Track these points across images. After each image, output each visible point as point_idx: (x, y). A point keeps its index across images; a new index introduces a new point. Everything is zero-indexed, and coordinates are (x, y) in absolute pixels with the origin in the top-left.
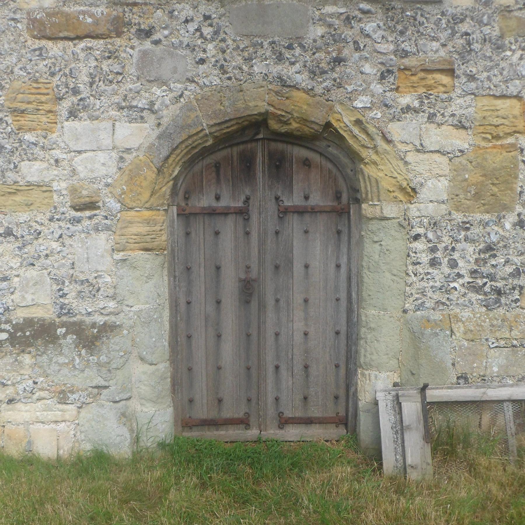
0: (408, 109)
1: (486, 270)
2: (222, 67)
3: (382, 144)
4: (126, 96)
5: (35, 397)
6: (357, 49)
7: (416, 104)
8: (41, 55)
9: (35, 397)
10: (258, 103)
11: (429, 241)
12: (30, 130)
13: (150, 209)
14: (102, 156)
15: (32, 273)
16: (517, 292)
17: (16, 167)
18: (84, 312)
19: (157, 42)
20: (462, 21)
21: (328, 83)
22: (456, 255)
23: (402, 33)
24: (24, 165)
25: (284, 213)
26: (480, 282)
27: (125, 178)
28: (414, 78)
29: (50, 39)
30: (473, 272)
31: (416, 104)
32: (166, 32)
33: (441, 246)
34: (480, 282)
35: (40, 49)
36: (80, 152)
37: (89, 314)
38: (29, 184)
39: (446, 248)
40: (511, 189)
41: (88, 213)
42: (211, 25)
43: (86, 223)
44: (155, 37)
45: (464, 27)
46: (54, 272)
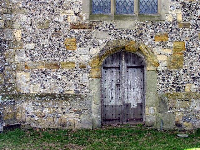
0: (157, 45)
1: (177, 82)
2: (115, 36)
3: (151, 53)
4: (92, 42)
5: (70, 112)
6: (145, 31)
7: (159, 44)
8: (73, 32)
9: (70, 112)
10: (122, 43)
11: (162, 76)
12: (70, 49)
13: (98, 68)
14: (87, 56)
15: (69, 83)
16: (184, 88)
17: (66, 58)
18: (81, 92)
19: (100, 30)
20: (170, 24)
21: (139, 39)
22: (169, 79)
23: (156, 27)
24: (68, 58)
25: (128, 68)
26: (175, 85)
27: (92, 61)
28: (159, 38)
29: (75, 29)
30: (173, 83)
31: (159, 44)
32: (102, 28)
33: (165, 77)
34: (175, 85)
35: (73, 31)
36: (82, 55)
37: (83, 93)
38: (70, 62)
39: (166, 77)
40: (182, 63)
41: (83, 69)
42: (112, 26)
43: (83, 71)
44: (99, 29)
45: (170, 26)
46: (75, 82)
